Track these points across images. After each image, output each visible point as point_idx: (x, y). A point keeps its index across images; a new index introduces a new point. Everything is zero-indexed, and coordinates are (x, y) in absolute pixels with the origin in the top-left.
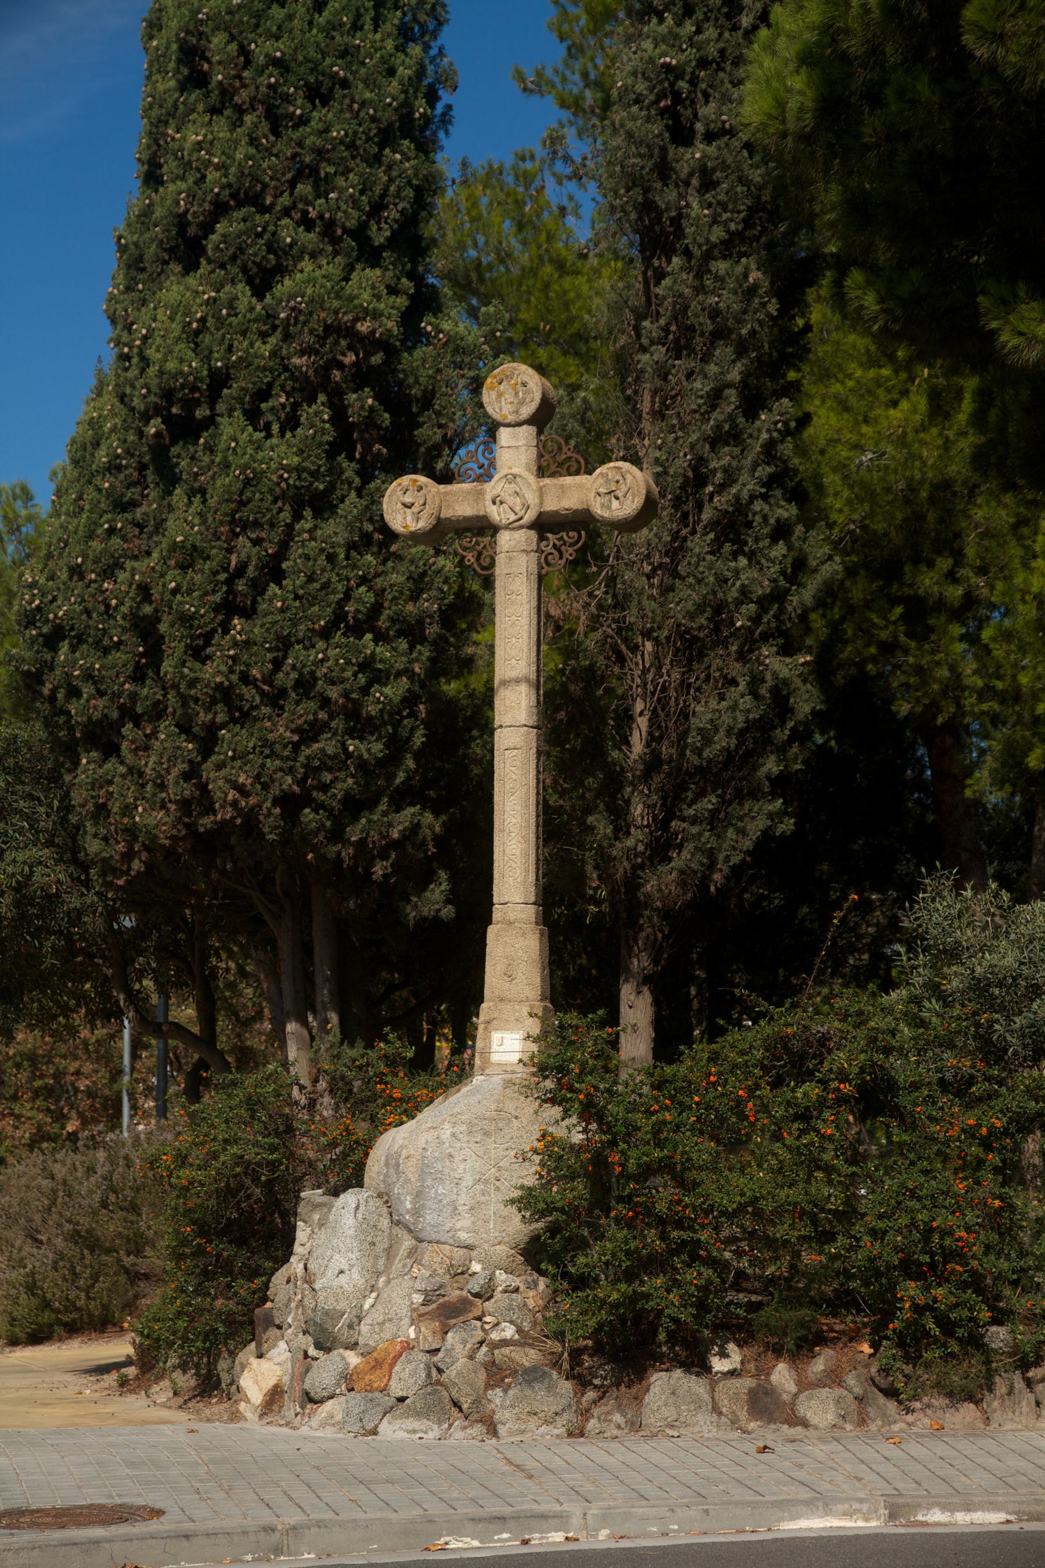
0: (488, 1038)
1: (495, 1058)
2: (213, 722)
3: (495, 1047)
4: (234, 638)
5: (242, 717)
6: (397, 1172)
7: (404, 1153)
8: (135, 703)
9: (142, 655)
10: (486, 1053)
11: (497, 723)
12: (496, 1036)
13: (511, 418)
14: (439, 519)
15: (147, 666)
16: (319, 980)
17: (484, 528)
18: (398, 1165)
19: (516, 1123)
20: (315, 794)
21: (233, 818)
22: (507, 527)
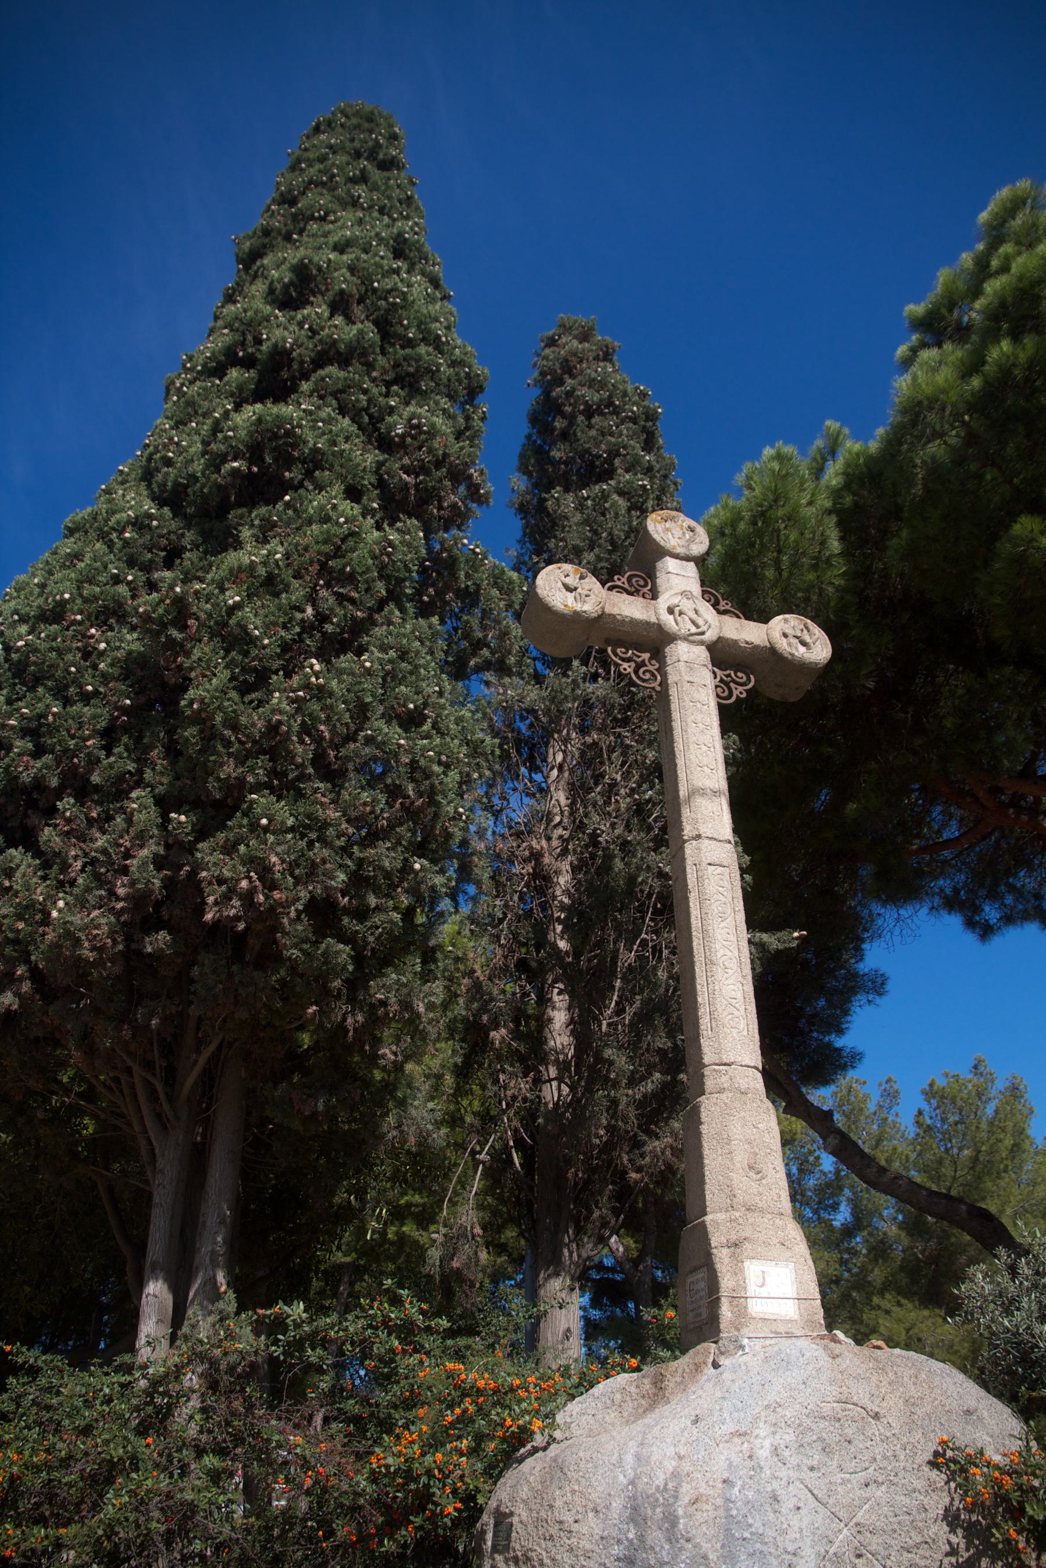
0: (738, 1271)
1: (755, 1308)
2: (241, 781)
3: (752, 1289)
4: (307, 677)
5: (284, 786)
6: (672, 1537)
7: (687, 1493)
8: (91, 771)
9: (124, 710)
10: (739, 1299)
11: (688, 831)
12: (753, 1269)
13: (679, 550)
14: (603, 612)
15: (126, 729)
16: (211, 1220)
17: (655, 642)
18: (671, 1520)
19: (874, 1428)
20: (346, 920)
21: (237, 918)
22: (685, 639)
